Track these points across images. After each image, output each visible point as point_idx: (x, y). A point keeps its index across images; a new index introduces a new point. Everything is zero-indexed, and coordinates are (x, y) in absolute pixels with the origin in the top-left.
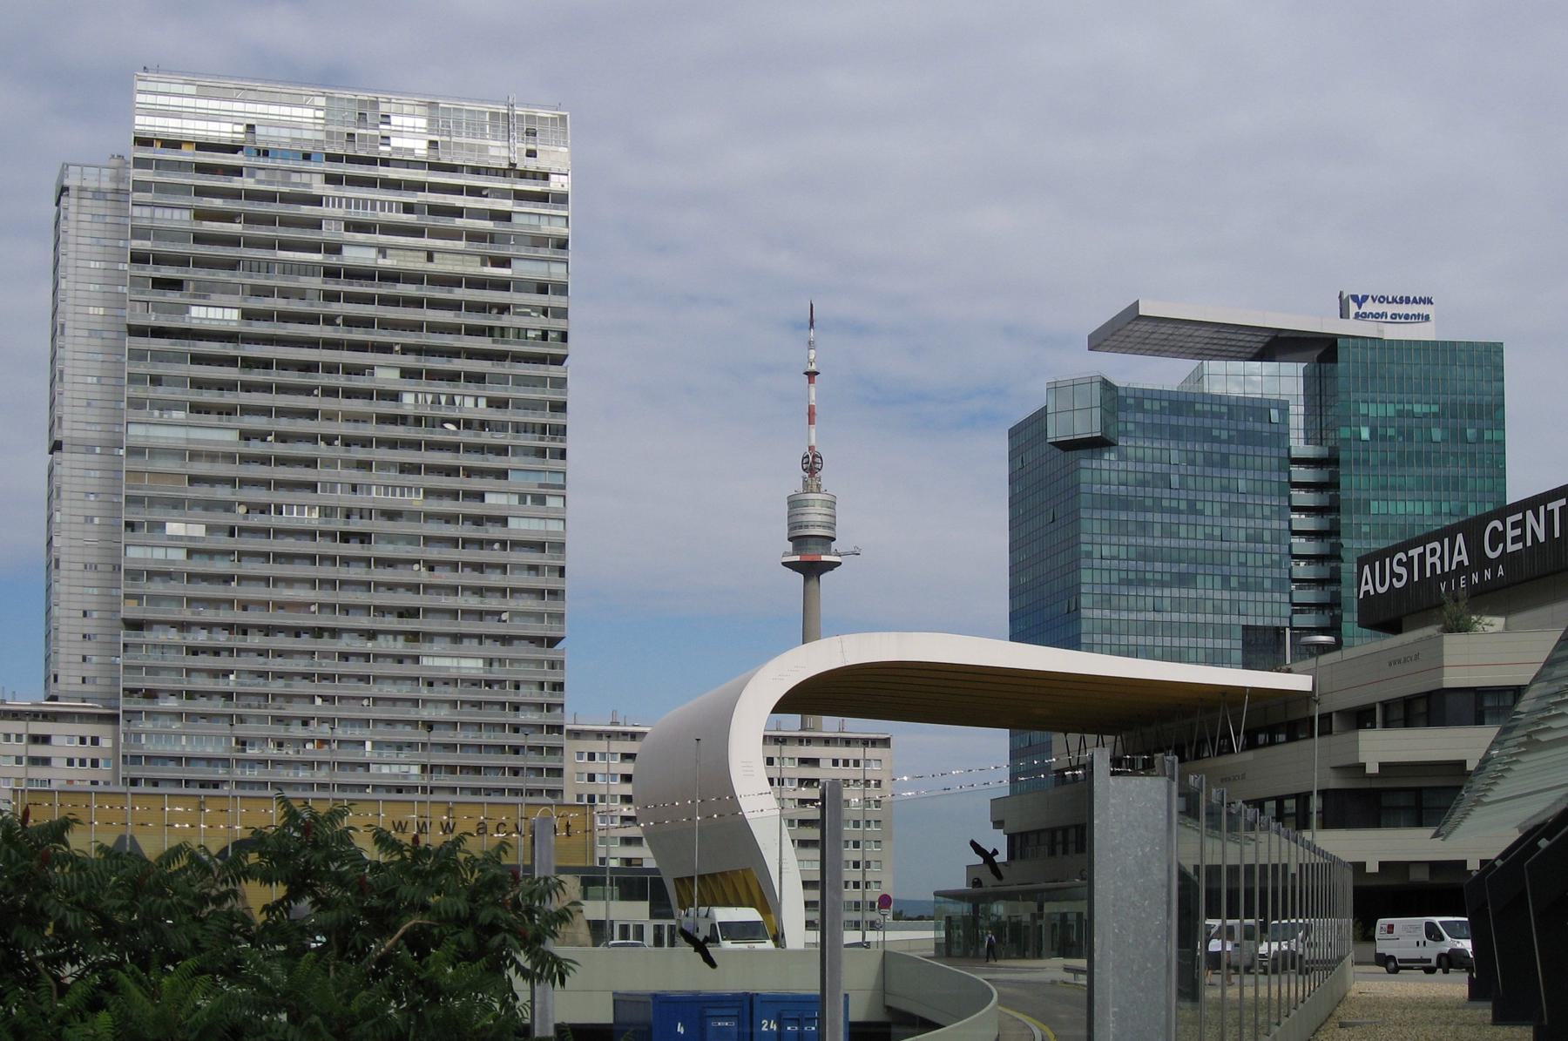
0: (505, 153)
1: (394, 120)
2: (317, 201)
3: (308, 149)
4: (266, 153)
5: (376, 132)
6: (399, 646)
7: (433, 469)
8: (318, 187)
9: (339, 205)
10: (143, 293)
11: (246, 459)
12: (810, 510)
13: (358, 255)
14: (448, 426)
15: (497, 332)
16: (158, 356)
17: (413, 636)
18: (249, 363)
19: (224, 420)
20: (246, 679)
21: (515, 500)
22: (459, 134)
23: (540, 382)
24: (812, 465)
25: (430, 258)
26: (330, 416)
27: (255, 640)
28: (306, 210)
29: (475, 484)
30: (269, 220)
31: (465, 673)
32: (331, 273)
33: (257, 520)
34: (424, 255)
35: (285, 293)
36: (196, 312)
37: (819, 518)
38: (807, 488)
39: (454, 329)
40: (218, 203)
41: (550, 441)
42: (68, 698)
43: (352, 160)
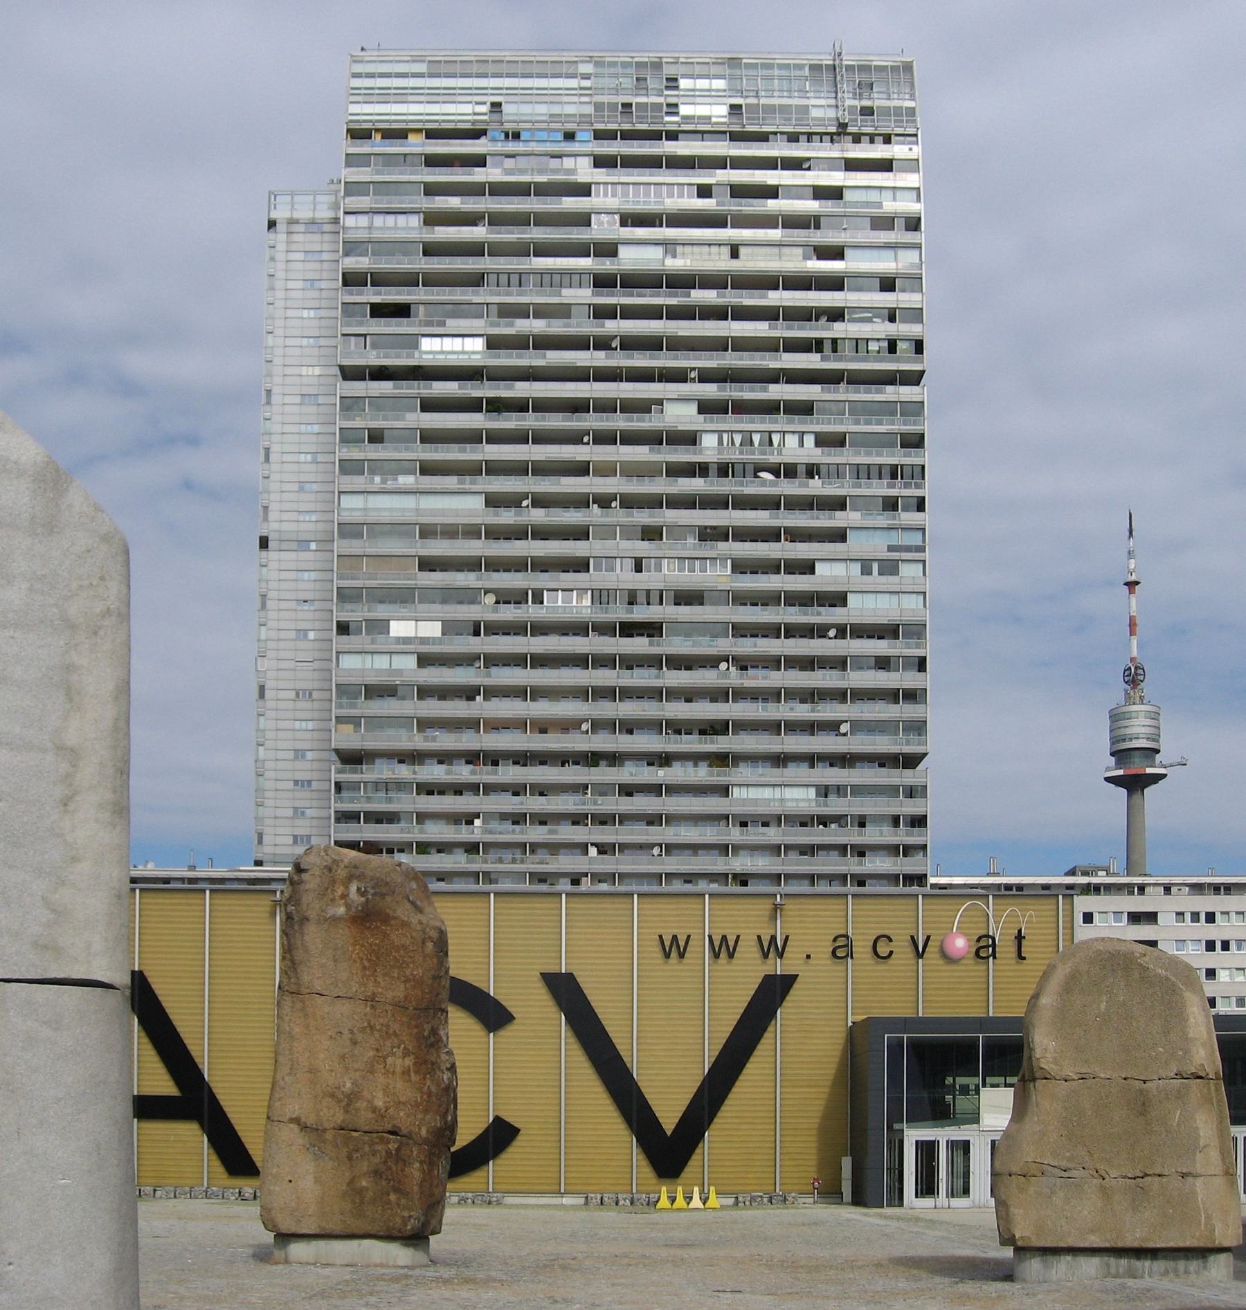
0: (831, 113)
1: (684, 83)
2: (584, 190)
3: (570, 127)
4: (516, 136)
5: (661, 100)
6: (702, 774)
7: (744, 534)
8: (584, 171)
9: (612, 195)
10: (361, 324)
11: (495, 533)
12: (1134, 722)
13: (637, 256)
14: (763, 475)
15: (827, 346)
16: (378, 402)
17: (721, 760)
18: (497, 406)
19: (468, 483)
20: (495, 825)
21: (856, 568)
22: (770, 92)
23: (888, 409)
24: (1133, 677)
25: (735, 254)
26: (607, 470)
27: (509, 773)
28: (570, 203)
29: (802, 550)
30: (521, 220)
31: (791, 808)
32: (602, 282)
33: (509, 613)
34: (726, 251)
35: (541, 312)
36: (427, 344)
37: (1143, 730)
38: (1129, 700)
39: (770, 346)
40: (454, 203)
41: (901, 486)
42: (275, 863)
43: (628, 136)
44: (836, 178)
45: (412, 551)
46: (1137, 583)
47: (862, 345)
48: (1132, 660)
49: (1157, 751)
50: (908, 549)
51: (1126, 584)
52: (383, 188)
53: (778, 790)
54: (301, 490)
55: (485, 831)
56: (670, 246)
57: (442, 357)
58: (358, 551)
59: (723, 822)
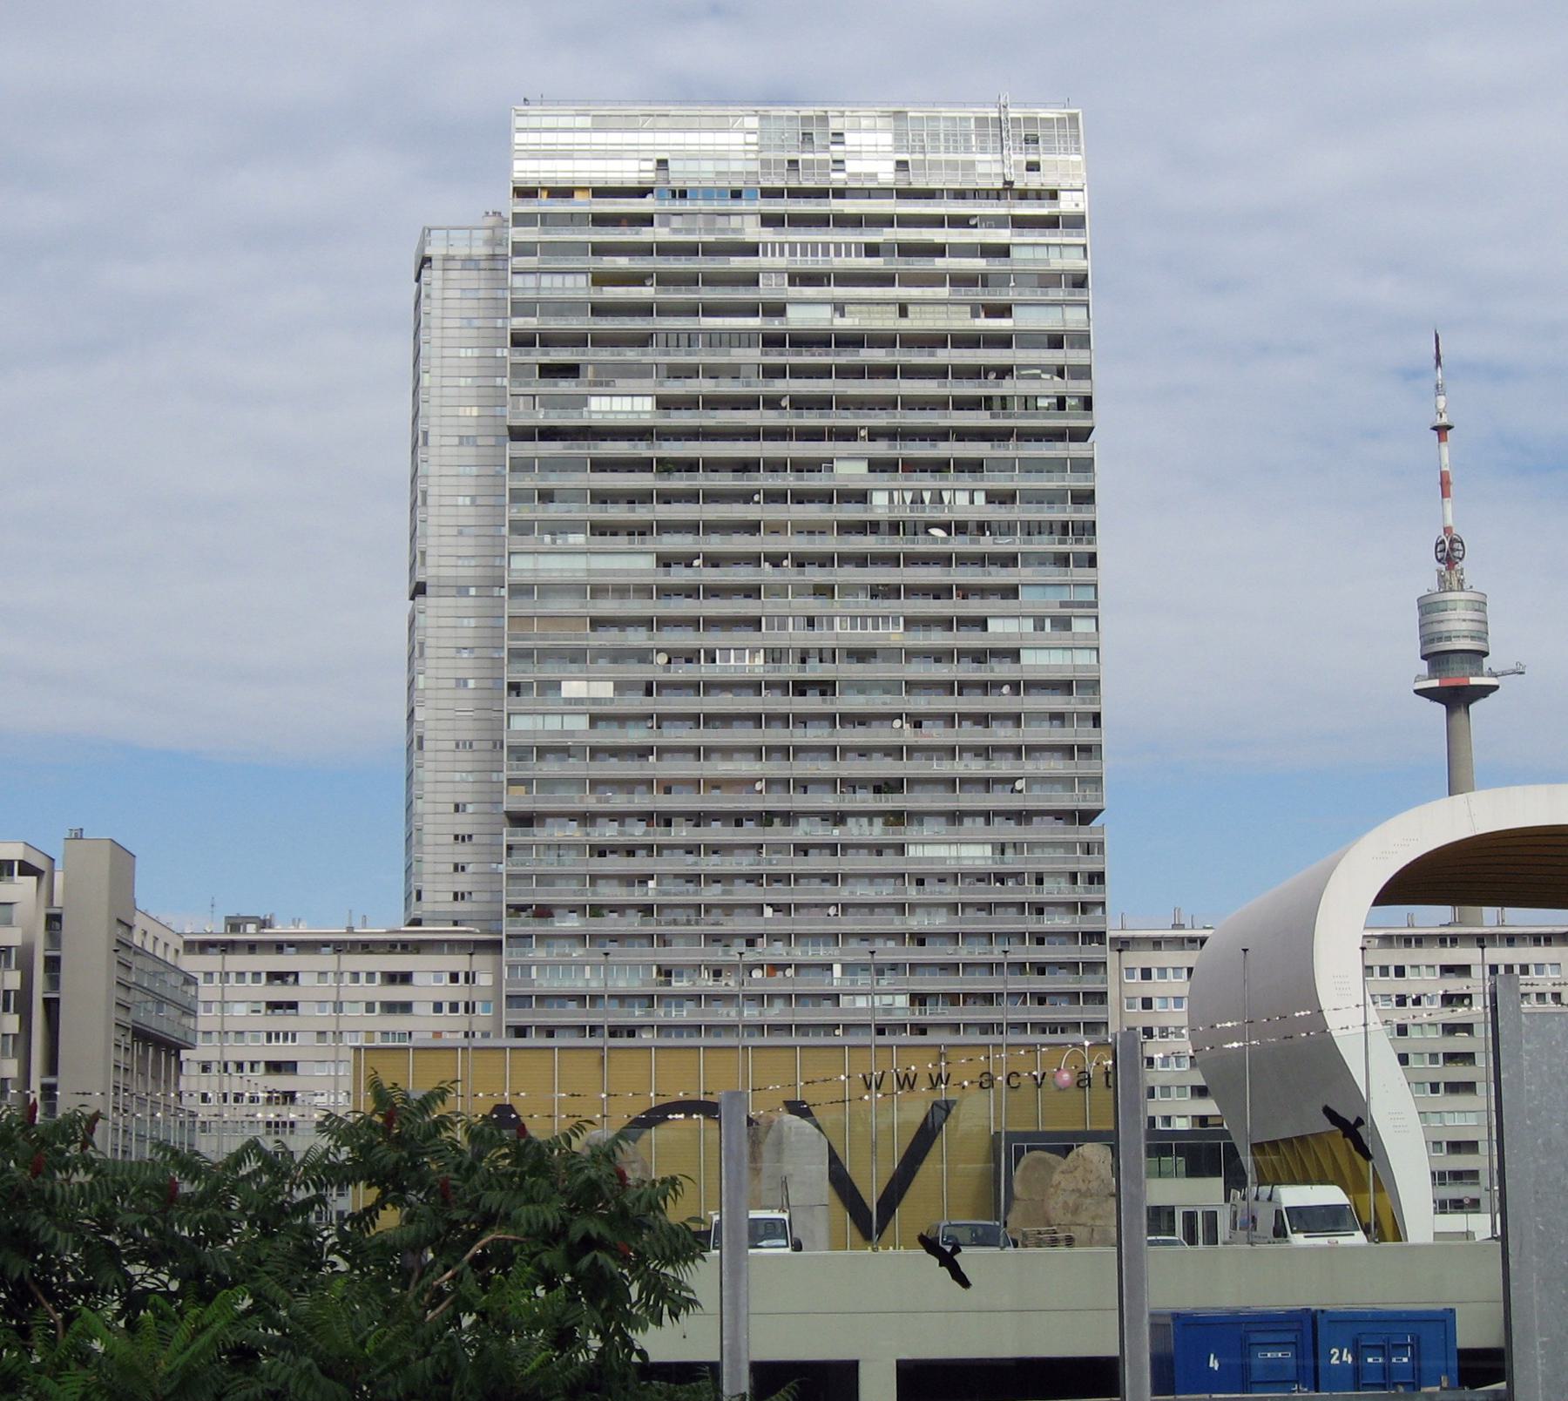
0: (997, 169)
2: (752, 250)
3: (738, 184)
4: (683, 194)
5: (827, 156)
6: (877, 832)
7: (914, 591)
8: (753, 232)
9: (780, 254)
10: (528, 385)
14: (934, 531)
15: (997, 404)
16: (551, 465)
17: (896, 818)
18: (667, 466)
20: (670, 886)
21: (1028, 625)
22: (936, 150)
23: (1058, 465)
25: (903, 312)
26: (777, 529)
28: (738, 263)
29: (974, 607)
30: (690, 280)
31: (967, 865)
33: (682, 672)
35: (713, 372)
36: (595, 403)
37: (1464, 626)
39: (939, 404)
41: (1074, 544)
42: (435, 921)
43: (795, 193)
44: (1003, 236)
45: (583, 611)
46: (1449, 428)
47: (1031, 403)
48: (1447, 530)
49: (1486, 654)
50: (1081, 605)
51: (1435, 428)
52: (551, 249)
53: (954, 847)
54: (460, 534)
55: (660, 893)
56: (839, 307)
57: (611, 416)
58: (528, 611)
59: (899, 881)
